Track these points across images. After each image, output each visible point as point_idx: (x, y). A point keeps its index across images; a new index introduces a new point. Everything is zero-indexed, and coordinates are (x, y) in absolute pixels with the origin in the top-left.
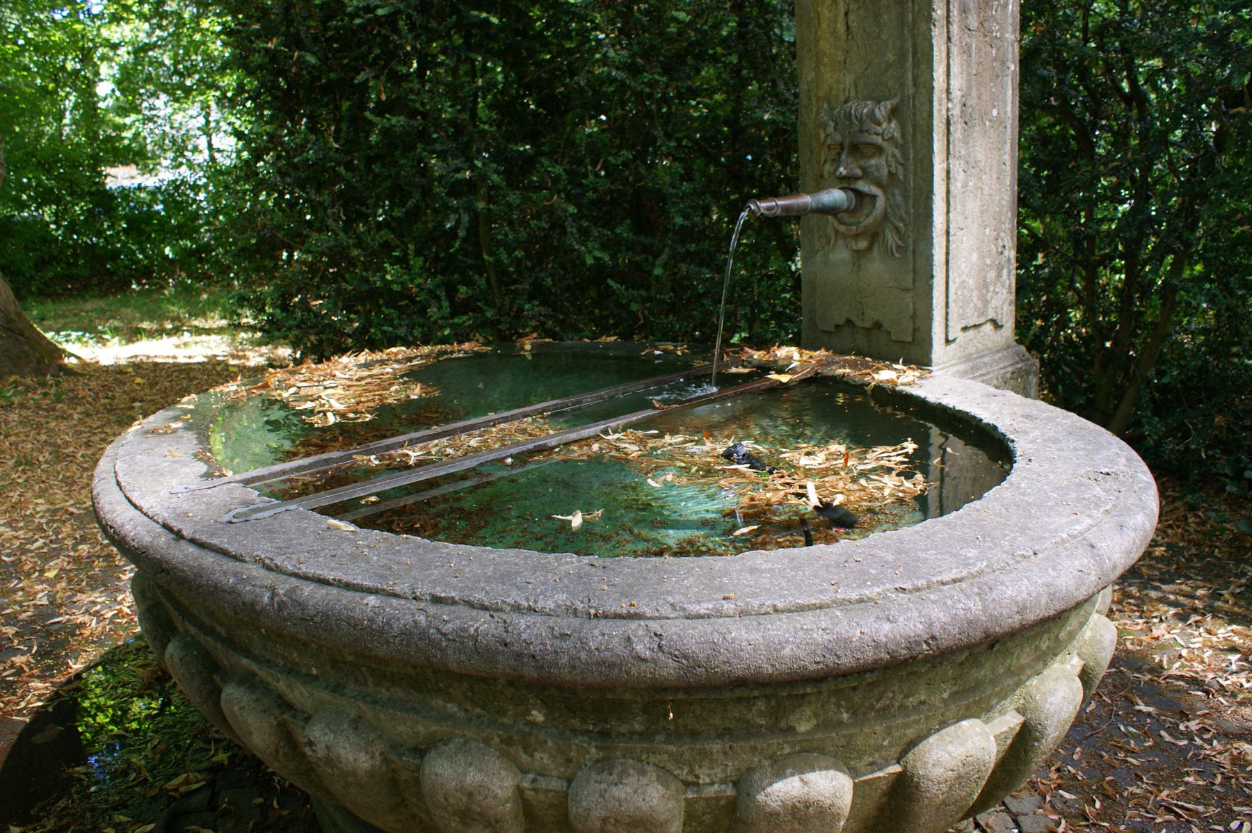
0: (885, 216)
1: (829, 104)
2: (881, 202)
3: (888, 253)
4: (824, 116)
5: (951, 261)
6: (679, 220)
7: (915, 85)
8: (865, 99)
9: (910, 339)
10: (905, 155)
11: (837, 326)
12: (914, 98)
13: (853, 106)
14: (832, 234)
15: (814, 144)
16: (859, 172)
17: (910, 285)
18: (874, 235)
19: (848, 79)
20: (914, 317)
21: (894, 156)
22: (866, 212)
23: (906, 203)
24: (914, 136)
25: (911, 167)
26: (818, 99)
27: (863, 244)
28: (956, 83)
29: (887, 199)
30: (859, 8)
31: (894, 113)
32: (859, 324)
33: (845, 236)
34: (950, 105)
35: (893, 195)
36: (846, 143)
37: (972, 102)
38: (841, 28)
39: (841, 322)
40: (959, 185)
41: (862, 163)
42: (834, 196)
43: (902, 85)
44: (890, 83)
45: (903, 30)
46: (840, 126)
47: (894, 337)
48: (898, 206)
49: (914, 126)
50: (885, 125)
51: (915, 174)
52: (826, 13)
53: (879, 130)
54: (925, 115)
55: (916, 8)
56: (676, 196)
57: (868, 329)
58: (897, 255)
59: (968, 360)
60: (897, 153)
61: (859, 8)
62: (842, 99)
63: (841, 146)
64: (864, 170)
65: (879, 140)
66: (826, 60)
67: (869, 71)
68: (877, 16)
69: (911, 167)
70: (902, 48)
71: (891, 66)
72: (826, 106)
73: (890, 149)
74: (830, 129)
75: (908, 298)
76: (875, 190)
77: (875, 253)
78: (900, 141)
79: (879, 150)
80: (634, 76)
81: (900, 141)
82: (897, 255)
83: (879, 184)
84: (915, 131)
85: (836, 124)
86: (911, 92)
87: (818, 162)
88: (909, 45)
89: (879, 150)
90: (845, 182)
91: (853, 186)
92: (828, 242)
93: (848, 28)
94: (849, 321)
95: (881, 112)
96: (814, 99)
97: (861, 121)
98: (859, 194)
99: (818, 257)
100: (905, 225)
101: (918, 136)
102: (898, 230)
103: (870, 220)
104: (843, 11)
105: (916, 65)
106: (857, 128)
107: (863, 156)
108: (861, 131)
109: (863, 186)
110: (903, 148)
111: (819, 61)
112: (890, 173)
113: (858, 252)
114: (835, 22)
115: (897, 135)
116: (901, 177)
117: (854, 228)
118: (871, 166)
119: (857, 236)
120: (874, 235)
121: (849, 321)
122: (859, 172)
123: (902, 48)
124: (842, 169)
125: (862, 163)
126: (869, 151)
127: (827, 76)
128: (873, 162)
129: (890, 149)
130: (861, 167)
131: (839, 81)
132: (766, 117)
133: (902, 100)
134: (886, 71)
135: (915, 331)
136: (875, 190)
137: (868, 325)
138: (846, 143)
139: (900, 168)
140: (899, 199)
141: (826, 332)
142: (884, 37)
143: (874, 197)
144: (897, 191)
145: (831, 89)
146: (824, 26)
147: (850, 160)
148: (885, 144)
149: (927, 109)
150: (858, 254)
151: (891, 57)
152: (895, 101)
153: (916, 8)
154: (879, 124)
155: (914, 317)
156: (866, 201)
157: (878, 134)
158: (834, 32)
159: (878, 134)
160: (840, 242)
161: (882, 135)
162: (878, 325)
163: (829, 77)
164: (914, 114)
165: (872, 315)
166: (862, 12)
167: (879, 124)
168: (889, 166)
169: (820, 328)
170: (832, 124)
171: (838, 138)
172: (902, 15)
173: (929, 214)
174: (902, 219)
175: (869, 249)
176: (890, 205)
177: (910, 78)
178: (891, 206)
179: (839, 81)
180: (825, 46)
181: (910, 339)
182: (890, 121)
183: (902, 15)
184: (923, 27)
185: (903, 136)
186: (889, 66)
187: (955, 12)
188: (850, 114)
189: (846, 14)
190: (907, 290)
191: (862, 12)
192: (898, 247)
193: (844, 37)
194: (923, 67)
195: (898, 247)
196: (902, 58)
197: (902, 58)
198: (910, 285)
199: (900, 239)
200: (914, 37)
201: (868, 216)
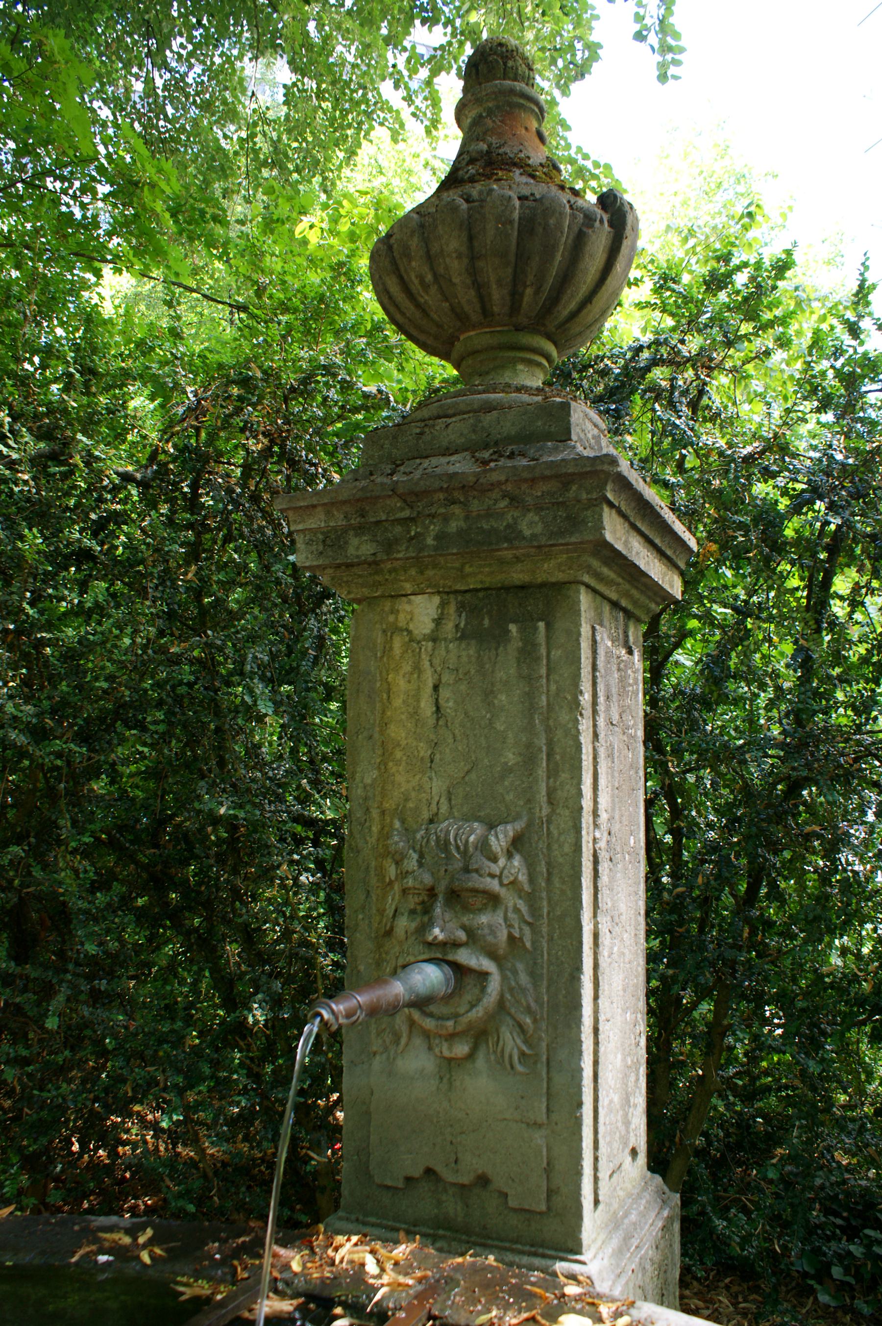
0: (501, 1004)
1: (403, 821)
2: (494, 985)
3: (503, 1064)
4: (397, 841)
5: (600, 1074)
6: (91, 948)
7: (550, 802)
8: (466, 818)
9: (543, 1207)
10: (534, 910)
11: (408, 1179)
12: (549, 822)
13: (449, 828)
14: (405, 1030)
15: (374, 881)
16: (462, 935)
17: (542, 1117)
18: (480, 1035)
19: (438, 786)
20: (549, 1170)
21: (517, 910)
22: (468, 997)
23: (536, 986)
24: (549, 880)
25: (545, 930)
26: (383, 813)
27: (461, 1049)
28: (604, 800)
29: (504, 978)
30: (458, 680)
31: (517, 844)
32: (449, 1177)
33: (427, 1035)
34: (598, 835)
35: (515, 972)
36: (441, 888)
37: (616, 828)
38: (427, 708)
39: (417, 1172)
40: (606, 954)
41: (465, 920)
42: (429, 976)
43: (529, 801)
44: (510, 797)
45: (532, 718)
46: (428, 859)
47: (512, 1203)
48: (523, 990)
49: (549, 864)
50: (502, 862)
51: (551, 939)
52: (401, 684)
53: (495, 869)
54: (567, 849)
55: (553, 687)
56: (87, 912)
57: (463, 1186)
58: (519, 1068)
59: (617, 1227)
60: (522, 905)
61: (458, 680)
62: (426, 815)
63: (432, 892)
64: (470, 932)
65: (494, 885)
66: (398, 754)
67: (473, 776)
68: (488, 695)
69: (545, 930)
70: (529, 745)
71: (510, 770)
72: (397, 824)
73: (510, 899)
74: (411, 862)
75: (539, 1138)
76: (487, 965)
77: (481, 1062)
78: (527, 887)
79: (493, 900)
80: (37, 743)
81: (527, 887)
82: (519, 1068)
83: (492, 955)
84: (549, 873)
85: (421, 856)
86: (544, 812)
87: (381, 912)
88: (541, 742)
89: (493, 900)
90: (440, 953)
91: (450, 957)
92: (397, 1042)
93: (438, 709)
94: (429, 1171)
95: (499, 841)
96: (375, 813)
97: (465, 853)
98: (459, 969)
99: (377, 1063)
100: (535, 1021)
101: (556, 882)
102: (521, 1027)
103: (478, 1013)
104: (430, 685)
105: (553, 772)
106: (459, 865)
107: (467, 909)
108: (467, 870)
109: (466, 957)
110: (531, 899)
111: (386, 755)
112: (511, 937)
113: (450, 1060)
114: (417, 698)
115: (523, 878)
116: (528, 945)
117: (450, 1023)
118: (480, 927)
119: (451, 1037)
120: (480, 1035)
121: (429, 1171)
122: (462, 935)
123: (529, 745)
124: (437, 931)
125: (465, 920)
126: (478, 901)
127: (400, 779)
128: (484, 919)
129: (510, 899)
130: (464, 928)
131: (420, 788)
132: (222, 811)
133: (530, 824)
134: (502, 778)
135: (551, 1193)
136: (487, 965)
137: (465, 1180)
138: (441, 888)
139: (527, 930)
140: (524, 979)
141: (388, 1188)
142: (500, 726)
143: (484, 975)
144: (520, 966)
145: (406, 800)
146: (398, 702)
147: (447, 916)
148: (503, 892)
149: (571, 839)
150: (451, 1064)
151: (511, 757)
152: (519, 825)
153: (553, 687)
154: (495, 860)
155: (549, 1170)
156: (470, 980)
157: (492, 876)
158: (415, 713)
159: (492, 876)
160: (418, 1041)
161: (500, 877)
162: (483, 1181)
163: (403, 780)
164: (549, 847)
165: (472, 1164)
166: (463, 687)
167: (495, 860)
168: (510, 926)
169: (378, 1180)
170: (415, 856)
171: (427, 879)
172: (530, 696)
173: (578, 1006)
174: (529, 1010)
175: (471, 1056)
176: (509, 988)
177: (544, 792)
178: (511, 990)
179: (420, 788)
180: (398, 732)
181: (543, 1207)
182: (510, 856)
183: (530, 696)
184: (564, 717)
185: (532, 880)
186: (508, 770)
187: (601, 699)
188: (447, 842)
189: (436, 688)
190: (538, 1126)
191: (463, 687)
192: (522, 1054)
193: (432, 721)
194: (564, 776)
195: (522, 1054)
196: (529, 760)
197: (529, 760)
198: (542, 1117)
199: (525, 1042)
200: (548, 730)
201: (473, 1006)
